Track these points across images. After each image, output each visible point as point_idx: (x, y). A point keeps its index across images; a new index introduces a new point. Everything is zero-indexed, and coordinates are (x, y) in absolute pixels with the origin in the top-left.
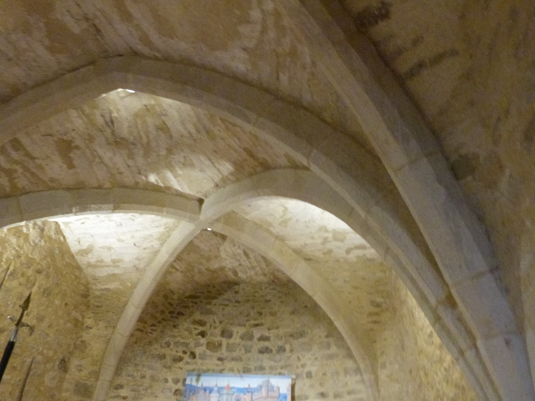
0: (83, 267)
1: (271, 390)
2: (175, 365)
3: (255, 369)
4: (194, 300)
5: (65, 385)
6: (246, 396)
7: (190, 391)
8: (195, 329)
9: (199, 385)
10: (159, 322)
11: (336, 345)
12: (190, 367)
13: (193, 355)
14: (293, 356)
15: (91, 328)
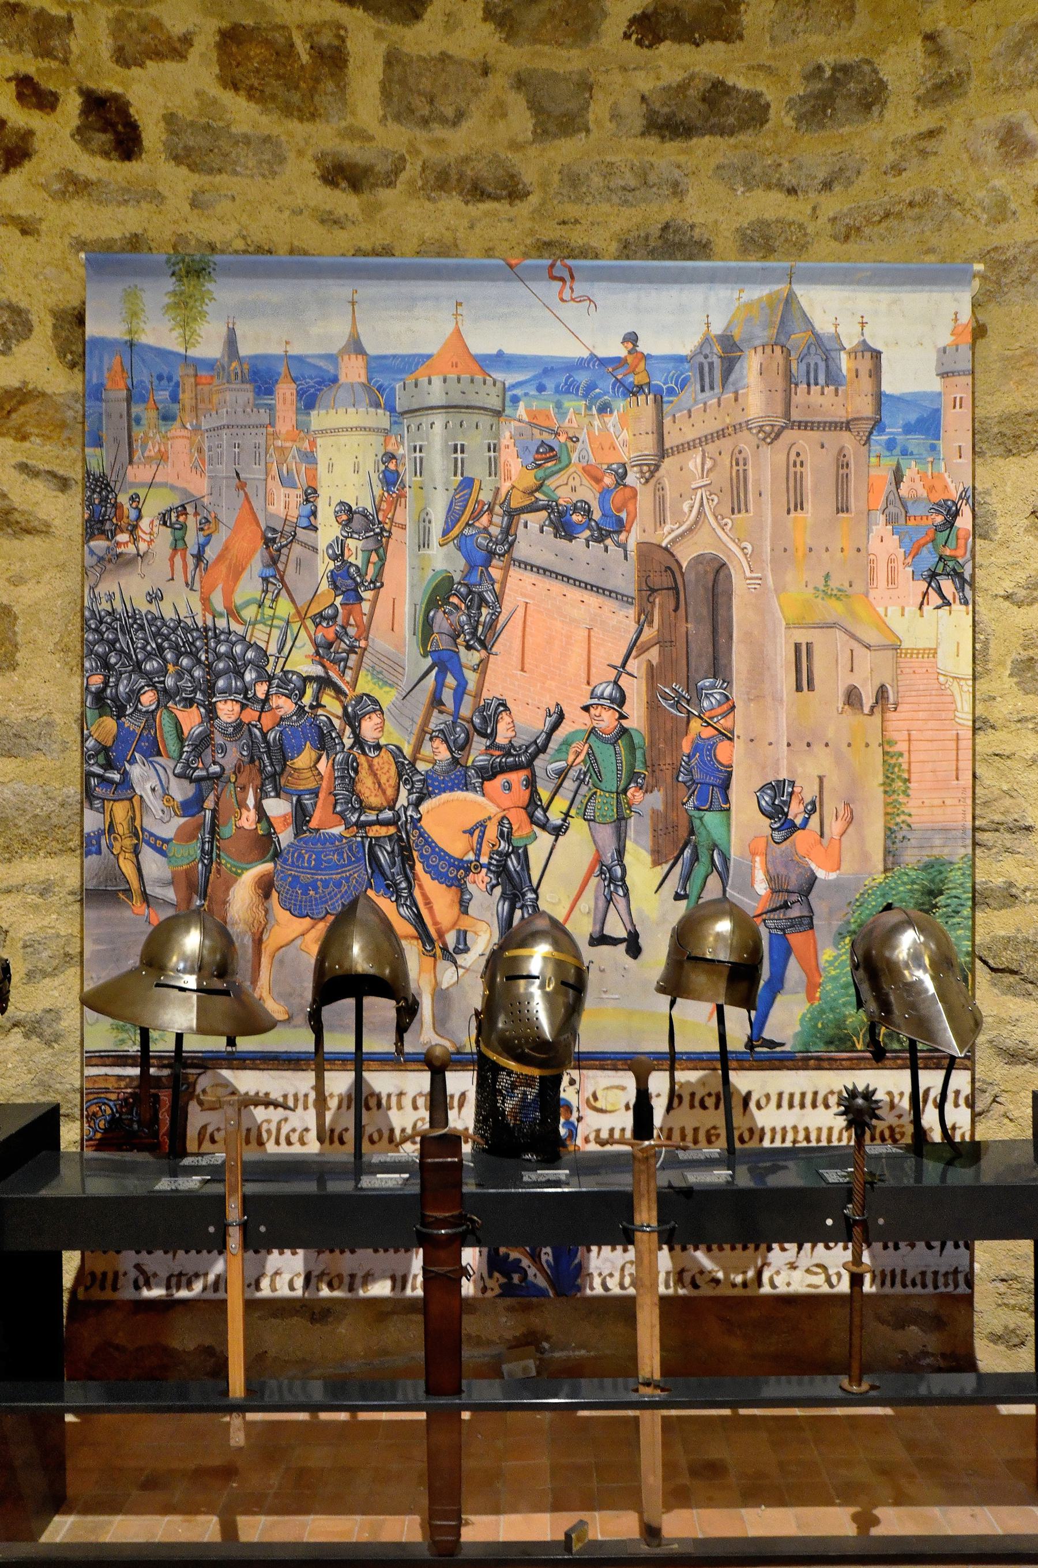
3: (627, 249)
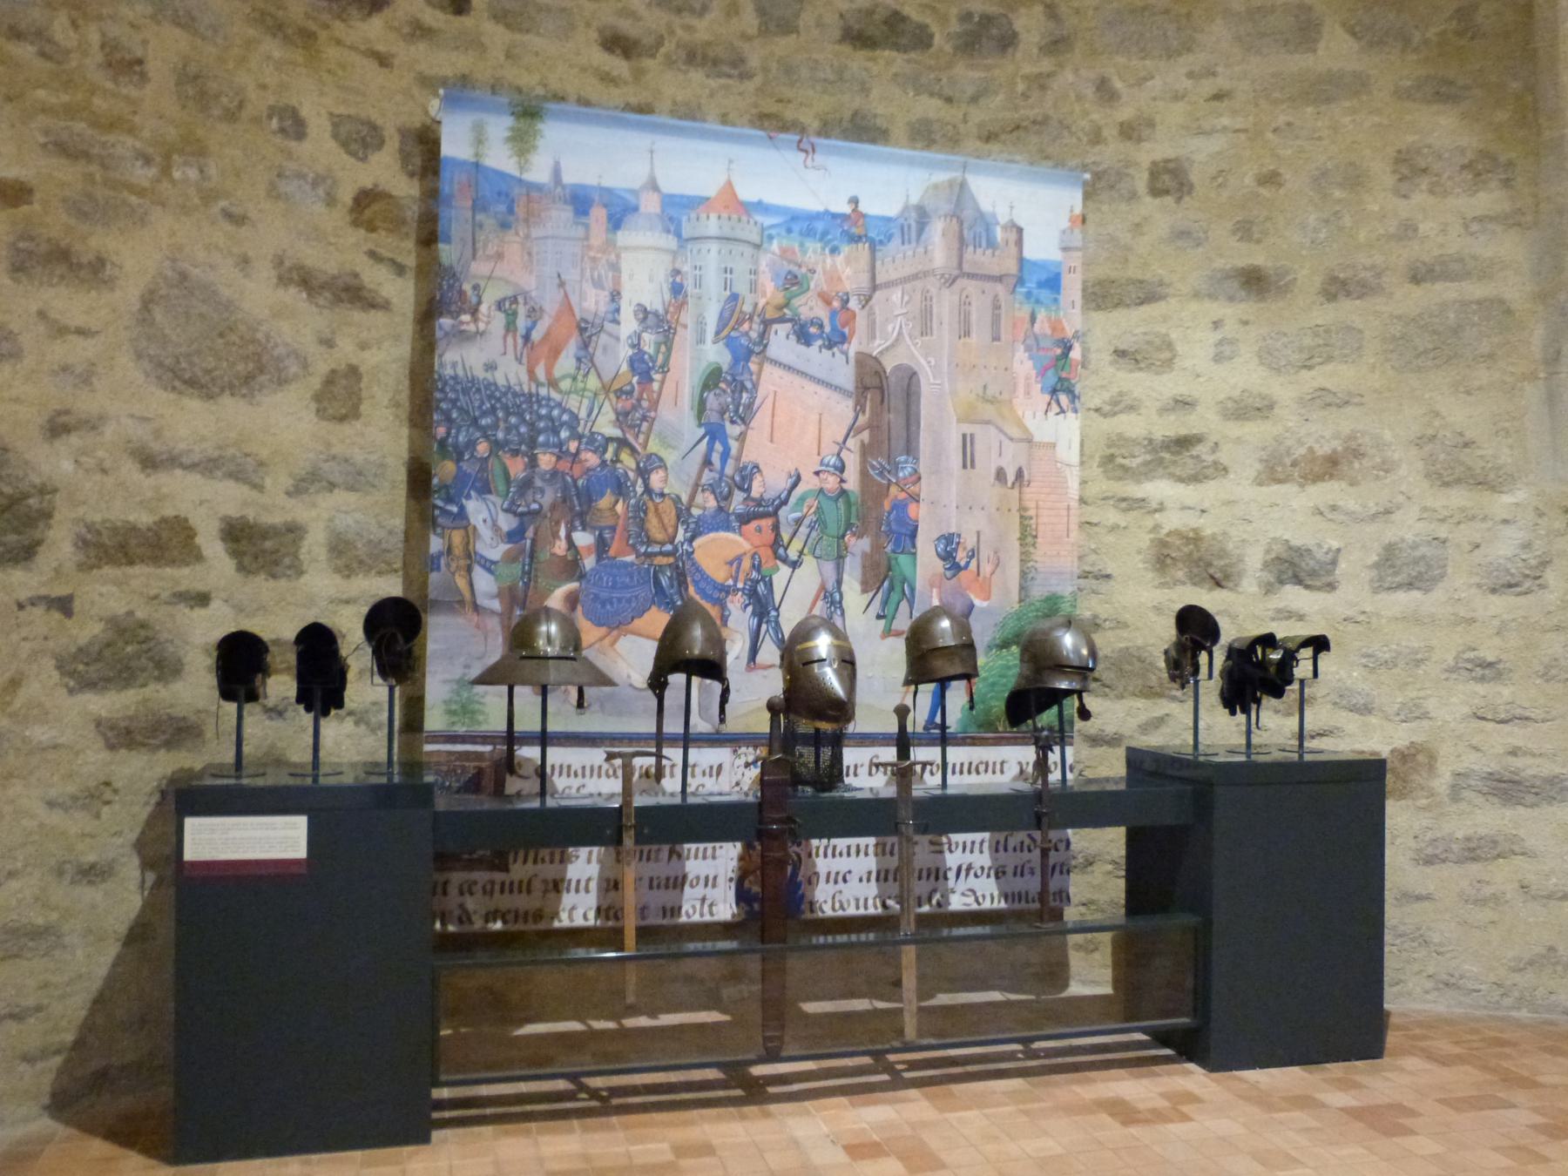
2: (339, 27)
7: (478, 206)
9: (539, 171)
12: (446, 62)
14: (1068, 76)
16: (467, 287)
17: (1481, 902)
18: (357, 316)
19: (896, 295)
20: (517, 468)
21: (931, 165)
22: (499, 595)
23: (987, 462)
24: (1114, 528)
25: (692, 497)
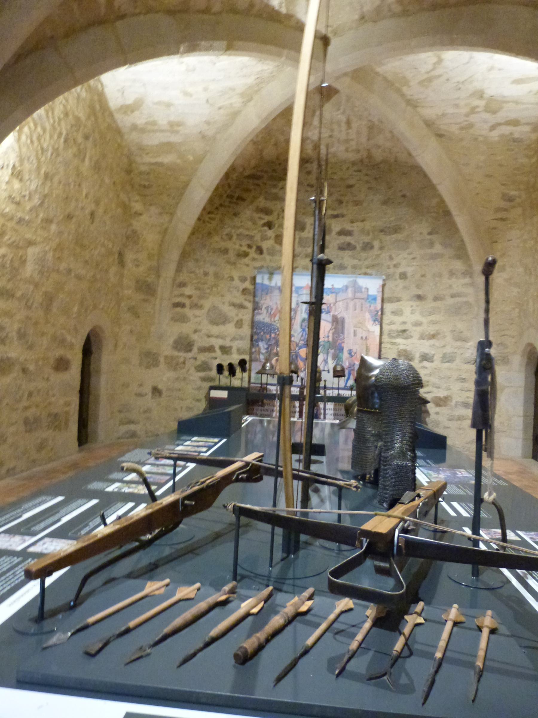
0: (124, 130)
1: (358, 292)
4: (256, 181)
5: (125, 282)
6: (329, 296)
7: (262, 291)
8: (260, 218)
9: (273, 284)
10: (217, 208)
11: (441, 244)
12: (258, 264)
13: (260, 250)
15: (141, 214)
16: (260, 305)
17: (460, 429)
18: (242, 310)
19: (341, 303)
20: (268, 337)
21: (349, 277)
22: (264, 359)
23: (359, 335)
24: (390, 348)
25: (299, 342)
